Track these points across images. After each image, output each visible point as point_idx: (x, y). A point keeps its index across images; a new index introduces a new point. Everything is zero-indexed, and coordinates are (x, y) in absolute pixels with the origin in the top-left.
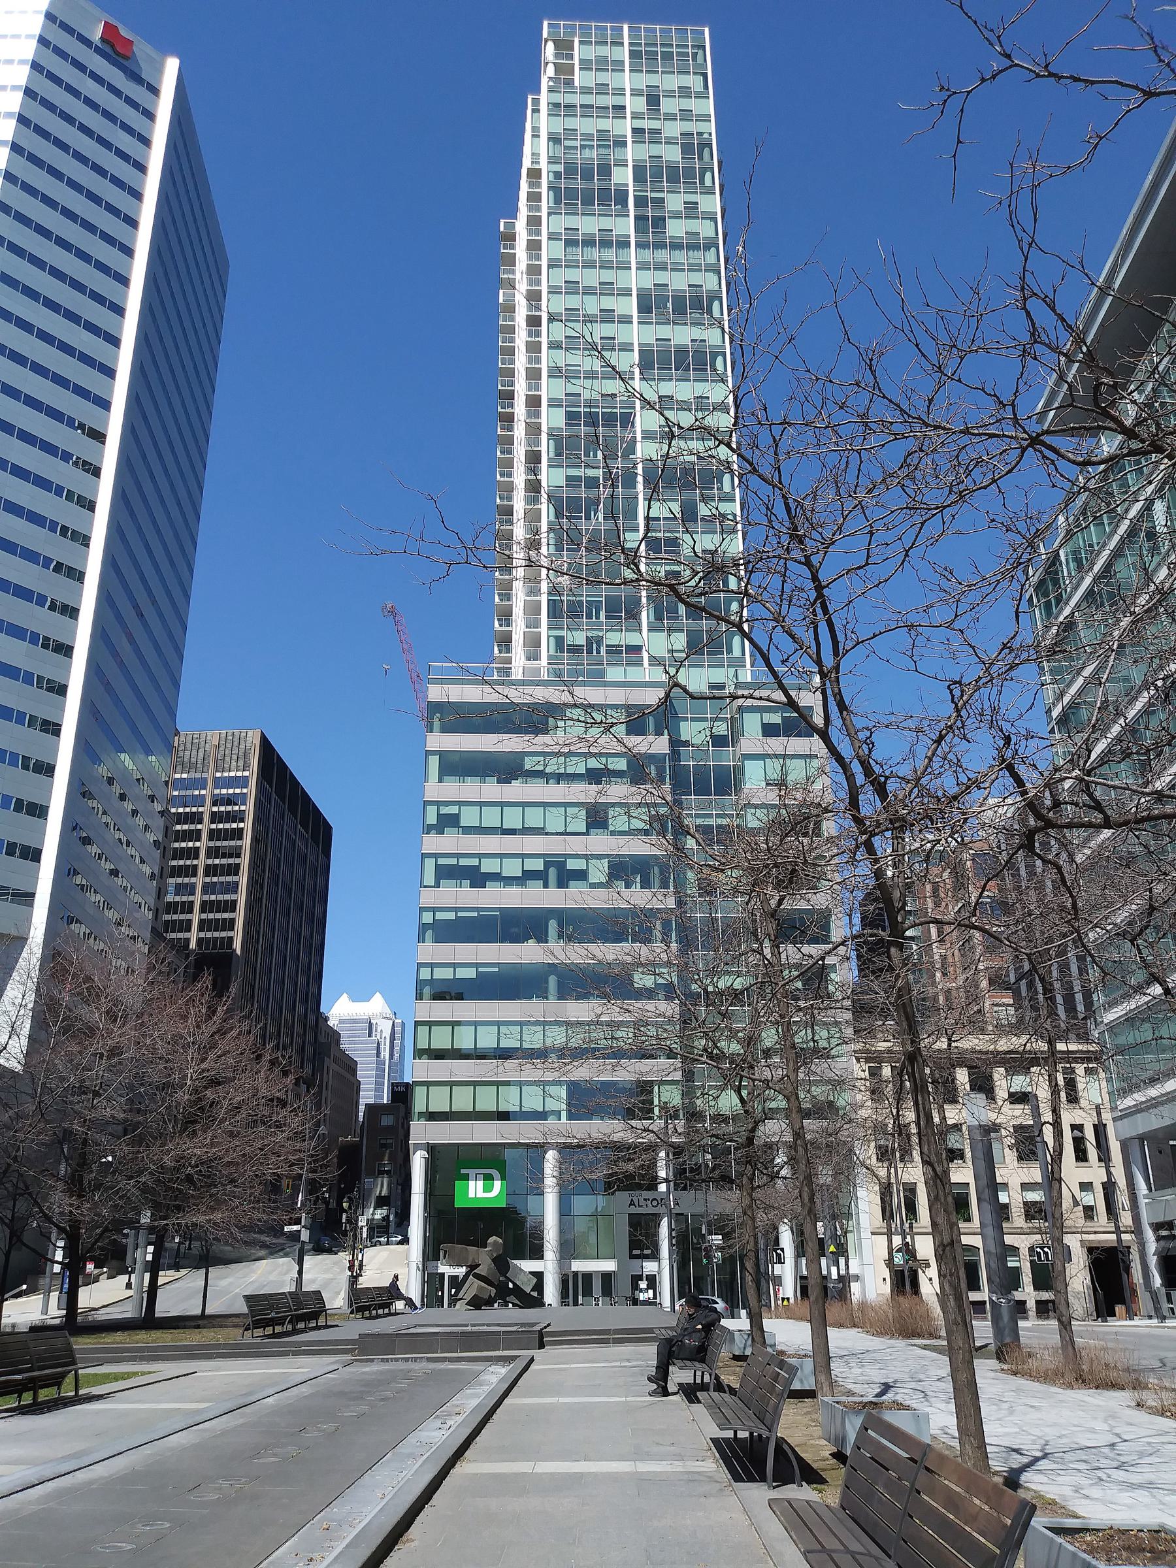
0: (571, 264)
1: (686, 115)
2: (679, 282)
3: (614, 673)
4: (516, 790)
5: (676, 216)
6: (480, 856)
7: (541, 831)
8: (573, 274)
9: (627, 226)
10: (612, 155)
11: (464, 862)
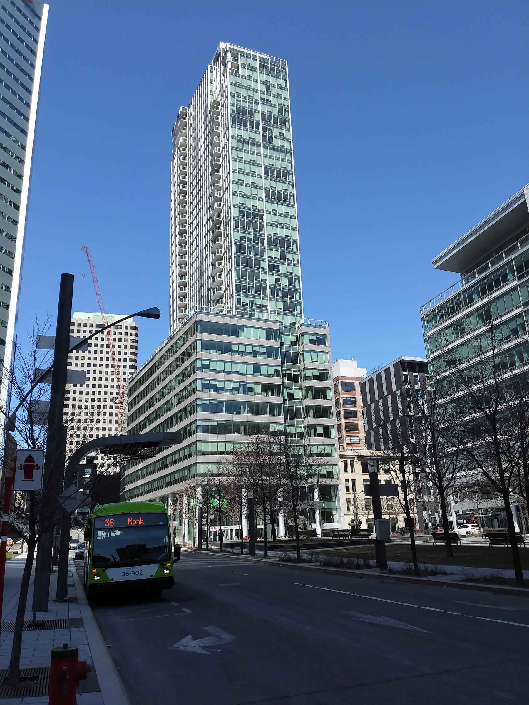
0: (240, 150)
1: (280, 96)
2: (278, 165)
3: (259, 315)
4: (228, 356)
5: (277, 137)
6: (217, 381)
7: (237, 373)
8: (241, 154)
9: (259, 138)
10: (254, 107)
11: (211, 382)
